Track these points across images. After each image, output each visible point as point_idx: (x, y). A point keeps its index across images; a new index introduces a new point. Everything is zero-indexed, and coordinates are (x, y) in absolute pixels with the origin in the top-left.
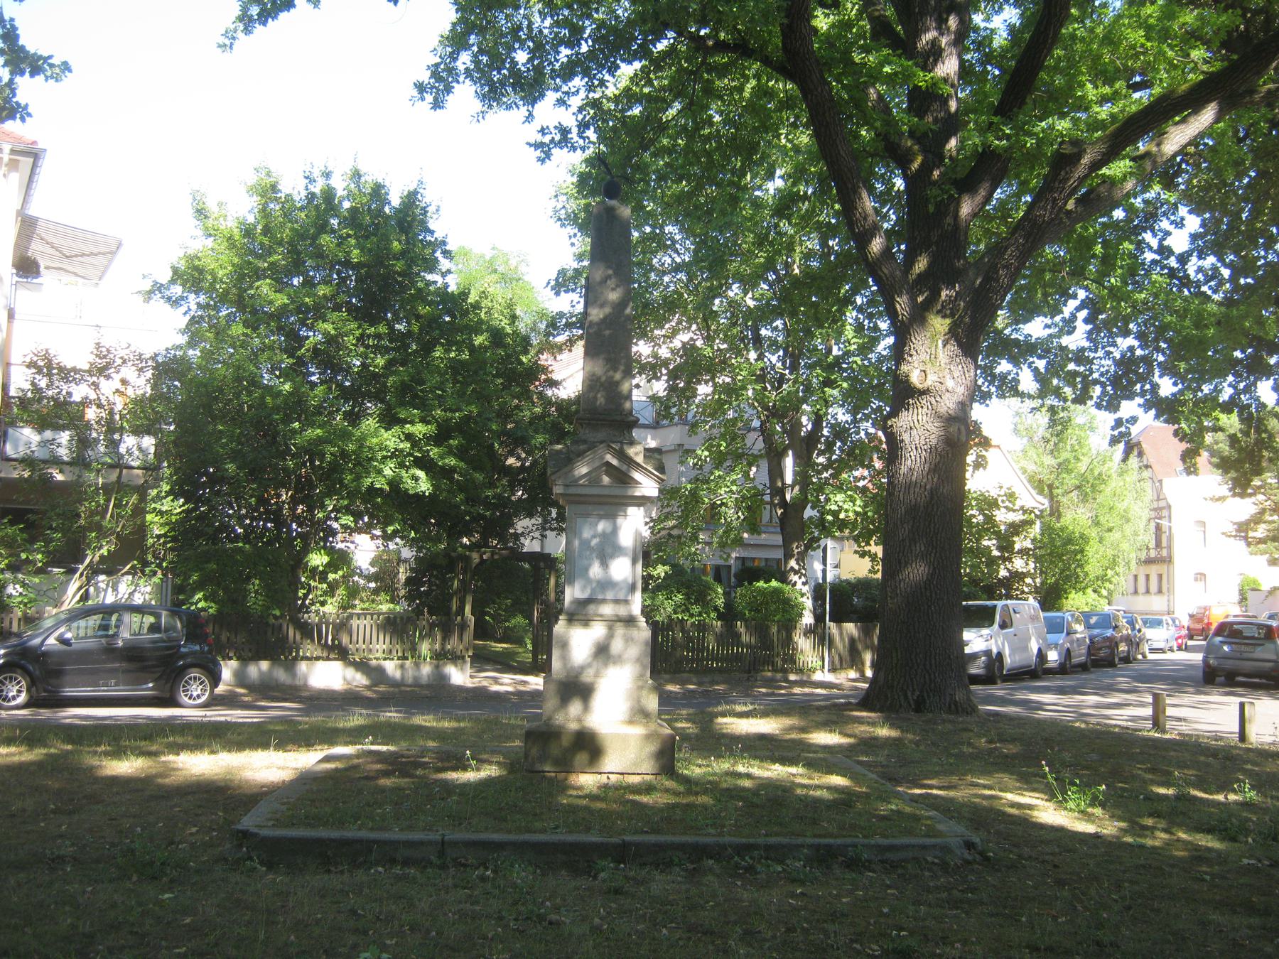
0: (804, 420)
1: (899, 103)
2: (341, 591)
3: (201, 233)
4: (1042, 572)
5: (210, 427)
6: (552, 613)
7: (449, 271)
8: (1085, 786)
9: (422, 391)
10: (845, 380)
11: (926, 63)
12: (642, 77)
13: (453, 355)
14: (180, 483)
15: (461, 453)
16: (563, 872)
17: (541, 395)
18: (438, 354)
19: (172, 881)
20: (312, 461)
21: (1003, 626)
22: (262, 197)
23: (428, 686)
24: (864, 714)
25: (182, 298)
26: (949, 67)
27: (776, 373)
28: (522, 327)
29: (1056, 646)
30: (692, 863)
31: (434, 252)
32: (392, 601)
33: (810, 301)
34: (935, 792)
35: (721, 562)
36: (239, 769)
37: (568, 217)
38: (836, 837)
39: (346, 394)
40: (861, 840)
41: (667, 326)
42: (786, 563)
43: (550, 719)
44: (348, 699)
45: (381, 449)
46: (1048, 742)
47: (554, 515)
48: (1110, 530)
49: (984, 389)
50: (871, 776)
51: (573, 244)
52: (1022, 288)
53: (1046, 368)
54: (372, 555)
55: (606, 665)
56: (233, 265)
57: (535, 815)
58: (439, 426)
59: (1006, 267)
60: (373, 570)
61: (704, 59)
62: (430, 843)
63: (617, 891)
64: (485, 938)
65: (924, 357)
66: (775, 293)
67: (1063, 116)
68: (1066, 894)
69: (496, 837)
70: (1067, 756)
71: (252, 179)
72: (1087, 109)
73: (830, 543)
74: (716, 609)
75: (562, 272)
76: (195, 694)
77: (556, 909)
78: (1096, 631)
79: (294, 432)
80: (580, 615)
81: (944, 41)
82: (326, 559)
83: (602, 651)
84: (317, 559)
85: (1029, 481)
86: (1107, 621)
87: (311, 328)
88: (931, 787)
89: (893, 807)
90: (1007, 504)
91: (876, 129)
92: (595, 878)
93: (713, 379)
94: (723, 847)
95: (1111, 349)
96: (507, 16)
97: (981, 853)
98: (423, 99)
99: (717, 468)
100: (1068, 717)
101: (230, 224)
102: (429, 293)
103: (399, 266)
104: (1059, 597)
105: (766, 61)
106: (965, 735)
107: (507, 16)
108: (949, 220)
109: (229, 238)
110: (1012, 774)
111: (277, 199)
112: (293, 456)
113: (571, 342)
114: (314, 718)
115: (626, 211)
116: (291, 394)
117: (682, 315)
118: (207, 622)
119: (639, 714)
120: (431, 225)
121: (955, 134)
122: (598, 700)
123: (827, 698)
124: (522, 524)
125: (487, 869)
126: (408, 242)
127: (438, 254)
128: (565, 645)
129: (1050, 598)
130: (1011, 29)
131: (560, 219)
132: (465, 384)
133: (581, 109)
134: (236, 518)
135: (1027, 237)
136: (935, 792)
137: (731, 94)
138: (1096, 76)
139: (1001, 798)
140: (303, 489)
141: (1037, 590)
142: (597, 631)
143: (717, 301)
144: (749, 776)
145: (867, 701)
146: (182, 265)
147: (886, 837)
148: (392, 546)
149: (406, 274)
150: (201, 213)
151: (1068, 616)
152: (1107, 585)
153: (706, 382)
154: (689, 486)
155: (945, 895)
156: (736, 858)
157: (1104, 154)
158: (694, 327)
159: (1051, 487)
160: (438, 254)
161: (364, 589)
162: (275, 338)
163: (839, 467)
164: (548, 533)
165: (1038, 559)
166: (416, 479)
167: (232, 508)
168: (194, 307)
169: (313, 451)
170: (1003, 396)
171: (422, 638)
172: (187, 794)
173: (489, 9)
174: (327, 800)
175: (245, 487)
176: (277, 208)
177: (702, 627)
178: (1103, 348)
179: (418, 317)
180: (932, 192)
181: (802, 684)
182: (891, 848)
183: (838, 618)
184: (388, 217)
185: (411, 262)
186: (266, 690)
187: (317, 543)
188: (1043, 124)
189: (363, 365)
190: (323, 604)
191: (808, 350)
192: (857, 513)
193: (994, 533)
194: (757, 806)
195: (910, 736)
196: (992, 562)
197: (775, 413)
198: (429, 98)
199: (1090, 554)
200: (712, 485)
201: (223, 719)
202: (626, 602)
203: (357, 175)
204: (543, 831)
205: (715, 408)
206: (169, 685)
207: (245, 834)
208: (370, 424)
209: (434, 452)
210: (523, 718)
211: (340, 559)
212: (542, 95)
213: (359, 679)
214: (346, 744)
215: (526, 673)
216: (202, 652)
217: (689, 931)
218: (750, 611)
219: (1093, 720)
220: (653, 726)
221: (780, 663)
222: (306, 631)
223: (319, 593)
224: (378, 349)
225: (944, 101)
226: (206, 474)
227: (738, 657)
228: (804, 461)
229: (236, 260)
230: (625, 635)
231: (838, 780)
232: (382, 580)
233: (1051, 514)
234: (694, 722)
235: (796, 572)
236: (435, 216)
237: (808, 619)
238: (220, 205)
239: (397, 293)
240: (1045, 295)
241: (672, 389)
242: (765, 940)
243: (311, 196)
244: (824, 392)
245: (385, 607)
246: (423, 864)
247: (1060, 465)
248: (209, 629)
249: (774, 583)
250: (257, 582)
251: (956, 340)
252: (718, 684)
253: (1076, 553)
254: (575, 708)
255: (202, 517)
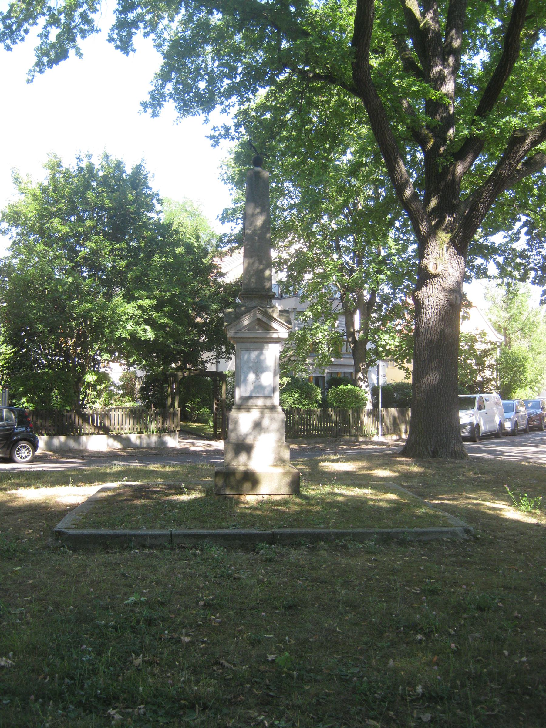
0: (365, 293)
1: (420, 107)
2: (104, 396)
3: (18, 192)
4: (501, 378)
5: (27, 304)
6: (227, 406)
7: (161, 211)
8: (531, 497)
9: (147, 280)
10: (389, 269)
11: (435, 84)
12: (272, 95)
13: (164, 259)
14: (10, 336)
15: (170, 316)
16: (239, 550)
17: (214, 281)
18: (155, 259)
19: (20, 560)
20: (85, 322)
21: (480, 408)
22: (52, 170)
23: (155, 448)
24: (404, 459)
25: (8, 230)
26: (449, 87)
27: (349, 266)
28: (202, 242)
29: (509, 419)
30: (312, 543)
31: (152, 200)
32: (133, 400)
33: (368, 225)
34: (445, 502)
35: (320, 375)
36: (55, 496)
37: (228, 178)
38: (393, 528)
39: (104, 283)
40: (406, 529)
41: (286, 240)
42: (356, 375)
43: (228, 465)
44: (111, 456)
45: (125, 315)
46: (508, 473)
47: (224, 350)
48: (539, 353)
49: (468, 274)
50: (410, 493)
51: (231, 194)
52: (491, 215)
53: (503, 261)
54: (121, 375)
55: (260, 433)
56: (37, 210)
57: (222, 519)
58: (158, 300)
59: (483, 203)
60: (121, 383)
61: (307, 84)
62: (164, 535)
63: (271, 560)
64: (198, 588)
65: (436, 256)
66: (348, 221)
67: (515, 115)
68: (522, 557)
69: (202, 531)
70: (519, 481)
71: (46, 160)
72: (528, 110)
73: (381, 363)
74: (317, 401)
75: (226, 210)
76: (24, 456)
77: (237, 570)
78: (532, 411)
79: (75, 305)
80: (245, 405)
81: (446, 71)
82: (95, 377)
83: (258, 426)
84: (90, 378)
85: (493, 326)
86: (538, 405)
87: (83, 245)
88: (443, 499)
89: (423, 511)
90: (481, 339)
91: (407, 124)
92: (258, 553)
93: (313, 270)
94: (329, 534)
95: (541, 250)
96: (192, 61)
97: (473, 536)
98: (145, 111)
99: (316, 321)
100: (518, 459)
101: (34, 187)
102: (150, 224)
103: (132, 208)
104: (510, 392)
105: (344, 85)
106: (461, 470)
107: (192, 61)
108: (450, 177)
109: (34, 195)
110: (488, 491)
111: (60, 171)
112: (75, 319)
113: (232, 250)
114: (92, 468)
115: (266, 174)
116: (72, 284)
117: (295, 234)
118: (29, 414)
119: (281, 461)
120: (150, 184)
121: (453, 126)
122: (255, 453)
123: (381, 451)
124: (206, 355)
125: (197, 549)
126: (137, 195)
127: (154, 201)
128: (236, 423)
129: (506, 392)
130: (485, 65)
131: (223, 180)
132: (172, 276)
133: (236, 116)
134: (43, 356)
135: (495, 185)
136: (445, 502)
137: (323, 105)
138: (533, 91)
139: (483, 505)
140: (80, 338)
141: (497, 388)
142: (255, 414)
143: (315, 226)
144: (341, 495)
145: (405, 452)
146: (7, 211)
147: (420, 527)
148: (132, 369)
149: (136, 213)
150: (17, 180)
151: (516, 403)
152: (538, 385)
153: (309, 272)
154: (300, 332)
155: (455, 559)
156: (337, 541)
157: (539, 137)
158: (302, 240)
159: (505, 329)
160: (154, 201)
161: (118, 394)
162: (62, 251)
163: (384, 319)
164: (220, 360)
165: (498, 370)
166: (145, 331)
167: (40, 350)
168: (15, 235)
169: (86, 316)
170: (479, 278)
171: (151, 421)
172: (24, 511)
173: (183, 58)
174: (104, 513)
175: (48, 338)
176: (61, 176)
177: (309, 412)
178: (536, 249)
179: (144, 238)
180: (440, 160)
181: (366, 443)
182: (423, 533)
183: (386, 406)
184: (125, 180)
185: (139, 206)
186: (64, 452)
187: (89, 368)
188: (504, 120)
189: (114, 267)
190: (94, 403)
191: (367, 253)
192: (396, 346)
193: (474, 356)
194: (347, 511)
195: (430, 471)
196: (473, 372)
197: (348, 289)
198: (150, 111)
199: (528, 367)
200: (314, 332)
201: (41, 469)
202: (271, 398)
203: (106, 156)
204: (227, 528)
205: (315, 287)
206: (9, 451)
207: (60, 533)
208: (118, 300)
209: (155, 315)
210: (211, 465)
211: (103, 378)
212: (213, 107)
213: (117, 445)
214: (112, 481)
215: (210, 439)
216: (27, 432)
217: (313, 582)
218: (336, 402)
219: (532, 461)
220: (287, 468)
221: (354, 431)
222: (85, 418)
223: (92, 397)
224: (121, 257)
225: (447, 108)
226: (25, 330)
227: (330, 429)
228: (366, 317)
229: (38, 207)
230: (270, 416)
231: (391, 496)
232: (127, 389)
233: (506, 345)
234: (307, 465)
235: (362, 380)
236: (152, 179)
237: (369, 406)
238: (28, 175)
239: (132, 224)
240: (504, 219)
241: (290, 276)
242: (355, 586)
243: (80, 169)
244: (376, 277)
245: (129, 404)
246: (161, 547)
247: (510, 316)
248: (30, 419)
249: (350, 386)
250: (57, 391)
251: (454, 246)
252: (319, 443)
253: (520, 366)
254: (243, 457)
255: (23, 356)
